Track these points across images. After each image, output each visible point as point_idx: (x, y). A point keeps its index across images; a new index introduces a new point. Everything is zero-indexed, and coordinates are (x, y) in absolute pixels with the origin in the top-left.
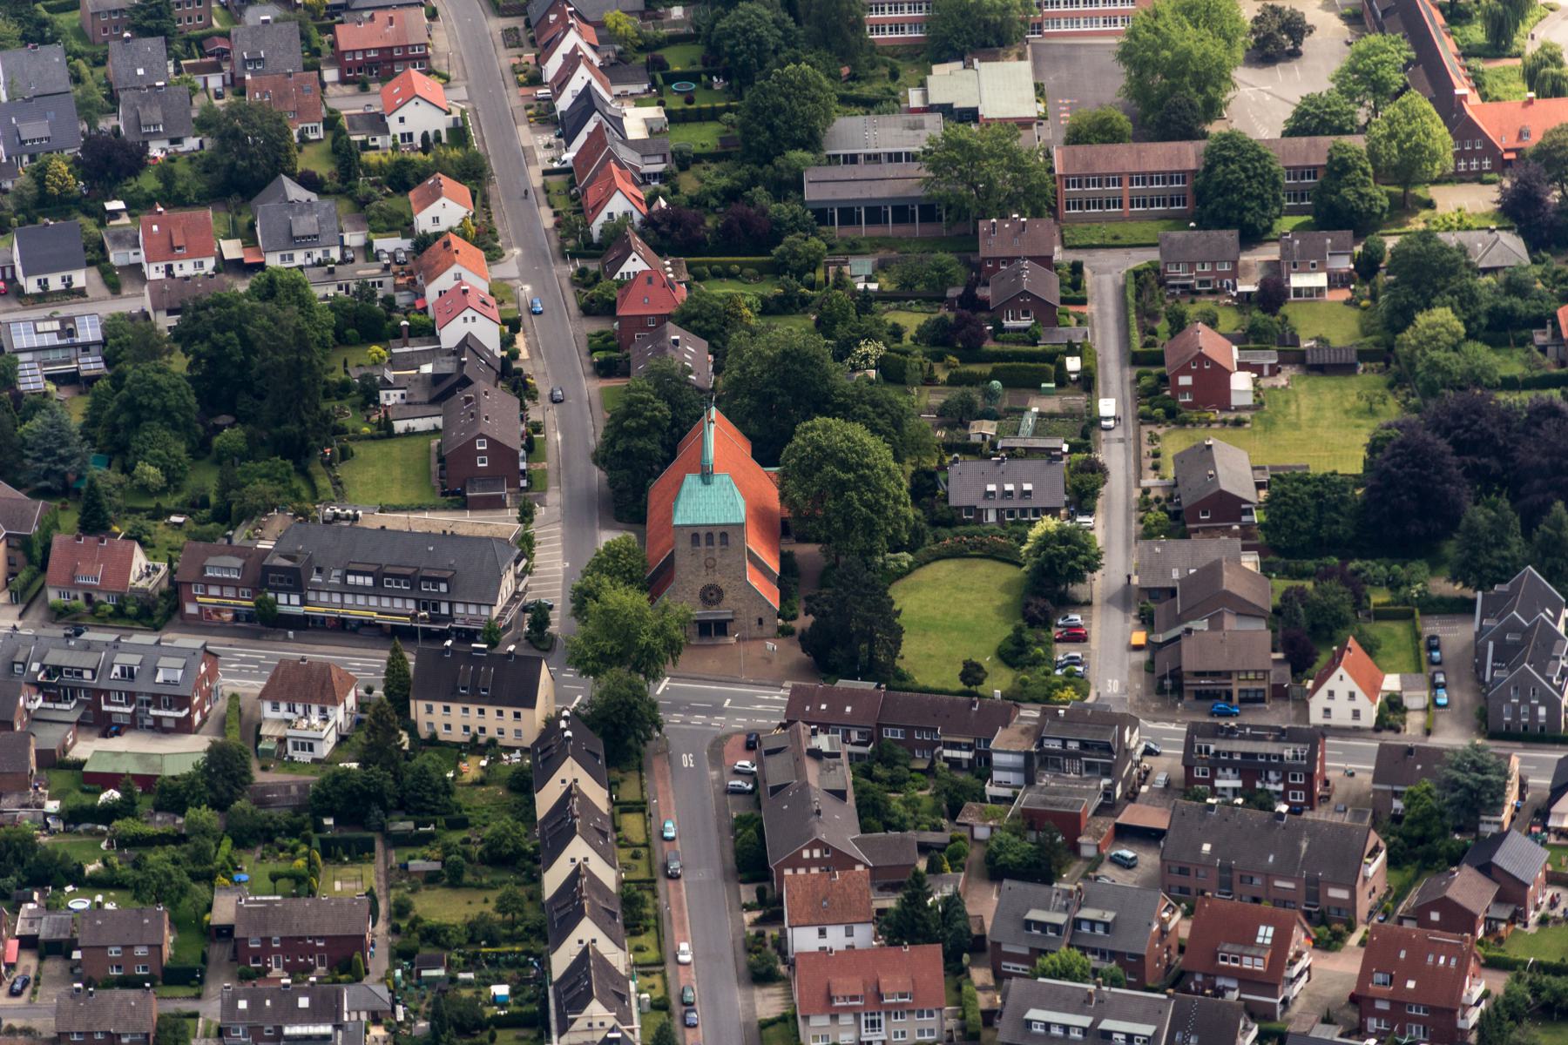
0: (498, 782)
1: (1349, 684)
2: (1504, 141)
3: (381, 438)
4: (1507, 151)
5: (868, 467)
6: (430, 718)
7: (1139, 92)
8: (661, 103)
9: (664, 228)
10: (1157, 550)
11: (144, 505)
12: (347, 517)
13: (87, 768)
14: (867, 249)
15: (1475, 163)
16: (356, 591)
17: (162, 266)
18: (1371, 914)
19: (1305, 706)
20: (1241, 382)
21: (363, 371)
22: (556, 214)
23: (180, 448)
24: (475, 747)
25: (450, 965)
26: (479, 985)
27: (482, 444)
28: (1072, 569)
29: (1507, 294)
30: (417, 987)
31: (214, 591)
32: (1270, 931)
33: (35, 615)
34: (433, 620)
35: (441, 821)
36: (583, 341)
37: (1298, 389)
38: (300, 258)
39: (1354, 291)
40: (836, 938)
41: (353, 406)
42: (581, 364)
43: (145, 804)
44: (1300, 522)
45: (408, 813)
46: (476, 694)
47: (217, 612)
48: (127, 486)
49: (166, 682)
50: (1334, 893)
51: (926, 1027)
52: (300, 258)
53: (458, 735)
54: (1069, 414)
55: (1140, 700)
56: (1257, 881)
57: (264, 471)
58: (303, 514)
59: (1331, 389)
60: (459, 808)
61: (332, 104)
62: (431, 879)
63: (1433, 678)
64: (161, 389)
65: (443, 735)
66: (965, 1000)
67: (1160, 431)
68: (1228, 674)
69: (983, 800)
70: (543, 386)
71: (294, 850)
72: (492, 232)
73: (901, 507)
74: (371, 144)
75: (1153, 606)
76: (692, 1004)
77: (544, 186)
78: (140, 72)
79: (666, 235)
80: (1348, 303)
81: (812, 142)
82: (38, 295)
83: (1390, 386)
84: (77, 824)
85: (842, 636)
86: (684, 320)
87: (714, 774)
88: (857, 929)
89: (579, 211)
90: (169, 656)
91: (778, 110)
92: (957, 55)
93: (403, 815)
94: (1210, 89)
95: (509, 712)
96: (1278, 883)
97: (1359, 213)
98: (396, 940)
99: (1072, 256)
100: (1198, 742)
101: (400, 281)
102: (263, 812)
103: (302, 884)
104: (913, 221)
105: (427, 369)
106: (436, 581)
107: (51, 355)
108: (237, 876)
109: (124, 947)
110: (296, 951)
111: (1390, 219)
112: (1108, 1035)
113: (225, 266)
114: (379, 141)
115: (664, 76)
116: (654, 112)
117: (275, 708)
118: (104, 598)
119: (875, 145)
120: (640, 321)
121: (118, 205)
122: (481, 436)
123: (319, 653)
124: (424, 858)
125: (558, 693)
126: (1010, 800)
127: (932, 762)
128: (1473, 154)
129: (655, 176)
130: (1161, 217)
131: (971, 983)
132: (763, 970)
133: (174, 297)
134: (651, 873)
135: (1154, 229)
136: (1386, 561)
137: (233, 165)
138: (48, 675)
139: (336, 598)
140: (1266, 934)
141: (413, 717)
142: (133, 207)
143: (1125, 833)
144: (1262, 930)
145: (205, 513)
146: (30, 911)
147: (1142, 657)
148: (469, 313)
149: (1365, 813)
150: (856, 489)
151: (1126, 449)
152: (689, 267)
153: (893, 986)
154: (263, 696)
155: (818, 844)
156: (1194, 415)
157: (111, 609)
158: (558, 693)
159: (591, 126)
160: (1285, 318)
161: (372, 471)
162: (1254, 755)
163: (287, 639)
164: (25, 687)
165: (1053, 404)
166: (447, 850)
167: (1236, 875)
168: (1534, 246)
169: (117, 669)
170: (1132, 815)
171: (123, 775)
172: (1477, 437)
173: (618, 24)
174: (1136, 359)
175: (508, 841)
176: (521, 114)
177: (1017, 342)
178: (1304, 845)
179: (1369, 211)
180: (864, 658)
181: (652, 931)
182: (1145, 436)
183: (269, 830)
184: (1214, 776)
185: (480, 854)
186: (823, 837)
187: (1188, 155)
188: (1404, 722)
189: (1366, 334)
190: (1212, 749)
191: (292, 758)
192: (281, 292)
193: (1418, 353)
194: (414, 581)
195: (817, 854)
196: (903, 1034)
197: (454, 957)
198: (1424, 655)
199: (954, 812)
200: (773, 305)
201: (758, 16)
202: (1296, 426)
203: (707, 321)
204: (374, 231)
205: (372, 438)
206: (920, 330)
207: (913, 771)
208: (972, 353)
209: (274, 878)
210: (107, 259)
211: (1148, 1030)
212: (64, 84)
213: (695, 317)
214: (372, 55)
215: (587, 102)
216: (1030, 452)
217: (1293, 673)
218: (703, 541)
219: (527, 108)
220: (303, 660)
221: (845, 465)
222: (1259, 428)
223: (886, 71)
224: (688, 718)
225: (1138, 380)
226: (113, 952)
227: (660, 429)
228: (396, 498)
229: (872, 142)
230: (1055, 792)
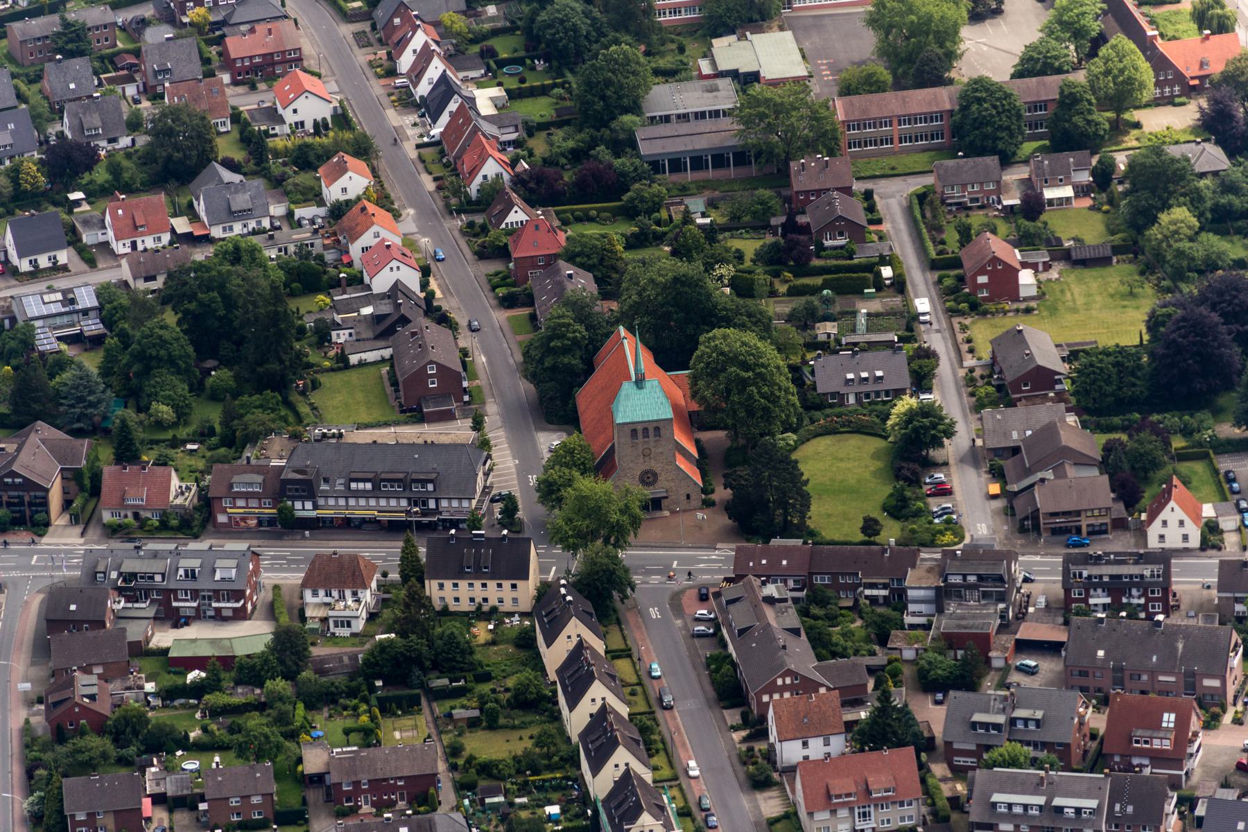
0: (507, 642)
1: (1180, 514)
2: (1190, 71)
3: (340, 369)
4: (1192, 78)
5: (763, 366)
6: (442, 593)
7: (887, 52)
8: (500, 84)
9: (532, 185)
10: (999, 417)
11: (162, 436)
12: (334, 436)
13: (172, 654)
14: (695, 191)
15: (1167, 90)
16: (358, 494)
17: (128, 242)
18: (1236, 697)
19: (1144, 535)
20: (1026, 278)
21: (314, 317)
22: (435, 179)
23: (182, 388)
24: (482, 614)
25: (506, 793)
26: (533, 807)
27: (432, 369)
28: (934, 437)
29: (1223, 193)
30: (483, 812)
31: (241, 503)
32: (1173, 717)
33: (94, 532)
34: (424, 514)
35: (470, 676)
36: (484, 280)
37: (1069, 280)
38: (238, 228)
39: (1094, 199)
40: (816, 748)
41: (310, 346)
42: (486, 299)
43: (227, 678)
44: (1102, 387)
45: (441, 672)
46: (478, 572)
47: (244, 519)
48: (147, 423)
49: (223, 579)
50: (1207, 682)
51: (906, 814)
52: (238, 228)
53: (465, 606)
54: (891, 313)
55: (1007, 538)
56: (1145, 677)
57: (258, 403)
58: (295, 437)
59: (1095, 278)
60: (480, 664)
61: (233, 102)
62: (473, 724)
63: (1237, 505)
64: (165, 342)
65: (453, 607)
66: (932, 790)
67: (967, 321)
68: (1078, 513)
69: (903, 628)
70: (461, 319)
71: (355, 708)
72: (387, 197)
73: (790, 397)
74: (271, 132)
75: (1001, 462)
76: (708, 810)
77: (420, 157)
78: (72, 86)
79: (537, 189)
80: (1091, 208)
81: (635, 108)
82: (30, 273)
83: (1142, 273)
84: (173, 700)
85: (761, 506)
86: (571, 258)
87: (679, 622)
88: (833, 739)
89: (455, 172)
90: (219, 557)
91: (608, 83)
92: (731, 31)
93: (438, 674)
94: (948, 44)
95: (507, 584)
96: (1161, 678)
97: (1087, 136)
98: (457, 776)
99: (869, 185)
100: (1074, 569)
101: (327, 242)
102: (324, 679)
103: (368, 737)
104: (729, 165)
105: (367, 311)
106: (423, 482)
107: (58, 321)
108: (314, 733)
109: (242, 797)
110: (381, 790)
111: (1110, 140)
112: (1060, 809)
113: (177, 238)
114: (278, 129)
115: (495, 62)
116: (496, 92)
117: (315, 594)
118: (149, 515)
119: (683, 107)
120: (532, 261)
121: (79, 195)
122: (431, 362)
123: (344, 547)
124: (463, 707)
125: (546, 565)
126: (927, 627)
127: (856, 601)
128: (1166, 82)
129: (509, 143)
130: (925, 150)
131: (933, 776)
132: (762, 778)
133: (146, 266)
134: (650, 707)
135: (920, 160)
136: (1177, 413)
137: (170, 158)
138: (124, 580)
139: (342, 502)
140: (1169, 719)
141: (428, 593)
142: (91, 196)
143: (1024, 646)
144: (1166, 716)
145: (214, 440)
146: (154, 773)
147: (999, 504)
148: (394, 264)
149: (1214, 617)
150: (755, 384)
151: (944, 338)
152: (557, 213)
153: (879, 784)
154: (304, 585)
155: (789, 673)
156: (991, 306)
157: (157, 524)
158: (546, 565)
159: (453, 106)
160: (1046, 223)
161: (339, 398)
162: (1120, 577)
163: (304, 538)
164: (111, 591)
165: (876, 306)
166: (483, 700)
167: (1127, 673)
168: (1231, 154)
169: (181, 572)
170: (1027, 631)
171: (209, 657)
172: (1237, 309)
173: (453, 22)
174: (934, 265)
175: (532, 689)
176: (385, 101)
177: (837, 258)
178: (1180, 646)
179: (1096, 134)
180: (779, 519)
181: (662, 753)
182: (957, 327)
183: (332, 693)
184: (1088, 595)
185: (508, 701)
186: (792, 667)
187: (942, 99)
188: (1222, 541)
189: (1113, 233)
190: (1085, 574)
191: (333, 634)
192: (245, 258)
193: (1164, 245)
194: (406, 483)
195: (788, 681)
196: (888, 821)
197: (509, 786)
198: (1226, 486)
199: (883, 640)
200: (632, 240)
201: (572, 9)
202: (1074, 310)
203: (588, 256)
204: (293, 203)
205: (332, 370)
206: (757, 254)
207: (841, 608)
208: (802, 269)
209: (347, 732)
210: (80, 240)
211: (1093, 804)
212: (13, 101)
213: (578, 254)
214: (257, 60)
215: (444, 89)
216: (872, 346)
217: (1127, 508)
218: (640, 435)
219: (390, 95)
220: (335, 553)
221: (745, 366)
222: (1045, 314)
223: (674, 46)
224: (647, 579)
225: (940, 281)
226: (234, 802)
227: (580, 348)
228: (364, 418)
229: (680, 104)
230: (963, 618)
